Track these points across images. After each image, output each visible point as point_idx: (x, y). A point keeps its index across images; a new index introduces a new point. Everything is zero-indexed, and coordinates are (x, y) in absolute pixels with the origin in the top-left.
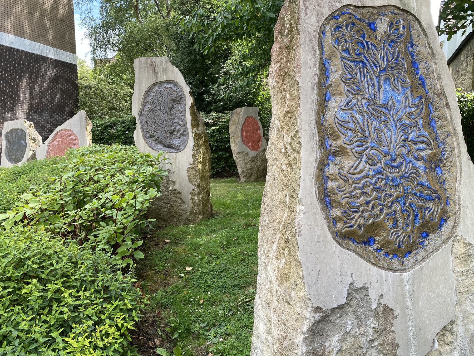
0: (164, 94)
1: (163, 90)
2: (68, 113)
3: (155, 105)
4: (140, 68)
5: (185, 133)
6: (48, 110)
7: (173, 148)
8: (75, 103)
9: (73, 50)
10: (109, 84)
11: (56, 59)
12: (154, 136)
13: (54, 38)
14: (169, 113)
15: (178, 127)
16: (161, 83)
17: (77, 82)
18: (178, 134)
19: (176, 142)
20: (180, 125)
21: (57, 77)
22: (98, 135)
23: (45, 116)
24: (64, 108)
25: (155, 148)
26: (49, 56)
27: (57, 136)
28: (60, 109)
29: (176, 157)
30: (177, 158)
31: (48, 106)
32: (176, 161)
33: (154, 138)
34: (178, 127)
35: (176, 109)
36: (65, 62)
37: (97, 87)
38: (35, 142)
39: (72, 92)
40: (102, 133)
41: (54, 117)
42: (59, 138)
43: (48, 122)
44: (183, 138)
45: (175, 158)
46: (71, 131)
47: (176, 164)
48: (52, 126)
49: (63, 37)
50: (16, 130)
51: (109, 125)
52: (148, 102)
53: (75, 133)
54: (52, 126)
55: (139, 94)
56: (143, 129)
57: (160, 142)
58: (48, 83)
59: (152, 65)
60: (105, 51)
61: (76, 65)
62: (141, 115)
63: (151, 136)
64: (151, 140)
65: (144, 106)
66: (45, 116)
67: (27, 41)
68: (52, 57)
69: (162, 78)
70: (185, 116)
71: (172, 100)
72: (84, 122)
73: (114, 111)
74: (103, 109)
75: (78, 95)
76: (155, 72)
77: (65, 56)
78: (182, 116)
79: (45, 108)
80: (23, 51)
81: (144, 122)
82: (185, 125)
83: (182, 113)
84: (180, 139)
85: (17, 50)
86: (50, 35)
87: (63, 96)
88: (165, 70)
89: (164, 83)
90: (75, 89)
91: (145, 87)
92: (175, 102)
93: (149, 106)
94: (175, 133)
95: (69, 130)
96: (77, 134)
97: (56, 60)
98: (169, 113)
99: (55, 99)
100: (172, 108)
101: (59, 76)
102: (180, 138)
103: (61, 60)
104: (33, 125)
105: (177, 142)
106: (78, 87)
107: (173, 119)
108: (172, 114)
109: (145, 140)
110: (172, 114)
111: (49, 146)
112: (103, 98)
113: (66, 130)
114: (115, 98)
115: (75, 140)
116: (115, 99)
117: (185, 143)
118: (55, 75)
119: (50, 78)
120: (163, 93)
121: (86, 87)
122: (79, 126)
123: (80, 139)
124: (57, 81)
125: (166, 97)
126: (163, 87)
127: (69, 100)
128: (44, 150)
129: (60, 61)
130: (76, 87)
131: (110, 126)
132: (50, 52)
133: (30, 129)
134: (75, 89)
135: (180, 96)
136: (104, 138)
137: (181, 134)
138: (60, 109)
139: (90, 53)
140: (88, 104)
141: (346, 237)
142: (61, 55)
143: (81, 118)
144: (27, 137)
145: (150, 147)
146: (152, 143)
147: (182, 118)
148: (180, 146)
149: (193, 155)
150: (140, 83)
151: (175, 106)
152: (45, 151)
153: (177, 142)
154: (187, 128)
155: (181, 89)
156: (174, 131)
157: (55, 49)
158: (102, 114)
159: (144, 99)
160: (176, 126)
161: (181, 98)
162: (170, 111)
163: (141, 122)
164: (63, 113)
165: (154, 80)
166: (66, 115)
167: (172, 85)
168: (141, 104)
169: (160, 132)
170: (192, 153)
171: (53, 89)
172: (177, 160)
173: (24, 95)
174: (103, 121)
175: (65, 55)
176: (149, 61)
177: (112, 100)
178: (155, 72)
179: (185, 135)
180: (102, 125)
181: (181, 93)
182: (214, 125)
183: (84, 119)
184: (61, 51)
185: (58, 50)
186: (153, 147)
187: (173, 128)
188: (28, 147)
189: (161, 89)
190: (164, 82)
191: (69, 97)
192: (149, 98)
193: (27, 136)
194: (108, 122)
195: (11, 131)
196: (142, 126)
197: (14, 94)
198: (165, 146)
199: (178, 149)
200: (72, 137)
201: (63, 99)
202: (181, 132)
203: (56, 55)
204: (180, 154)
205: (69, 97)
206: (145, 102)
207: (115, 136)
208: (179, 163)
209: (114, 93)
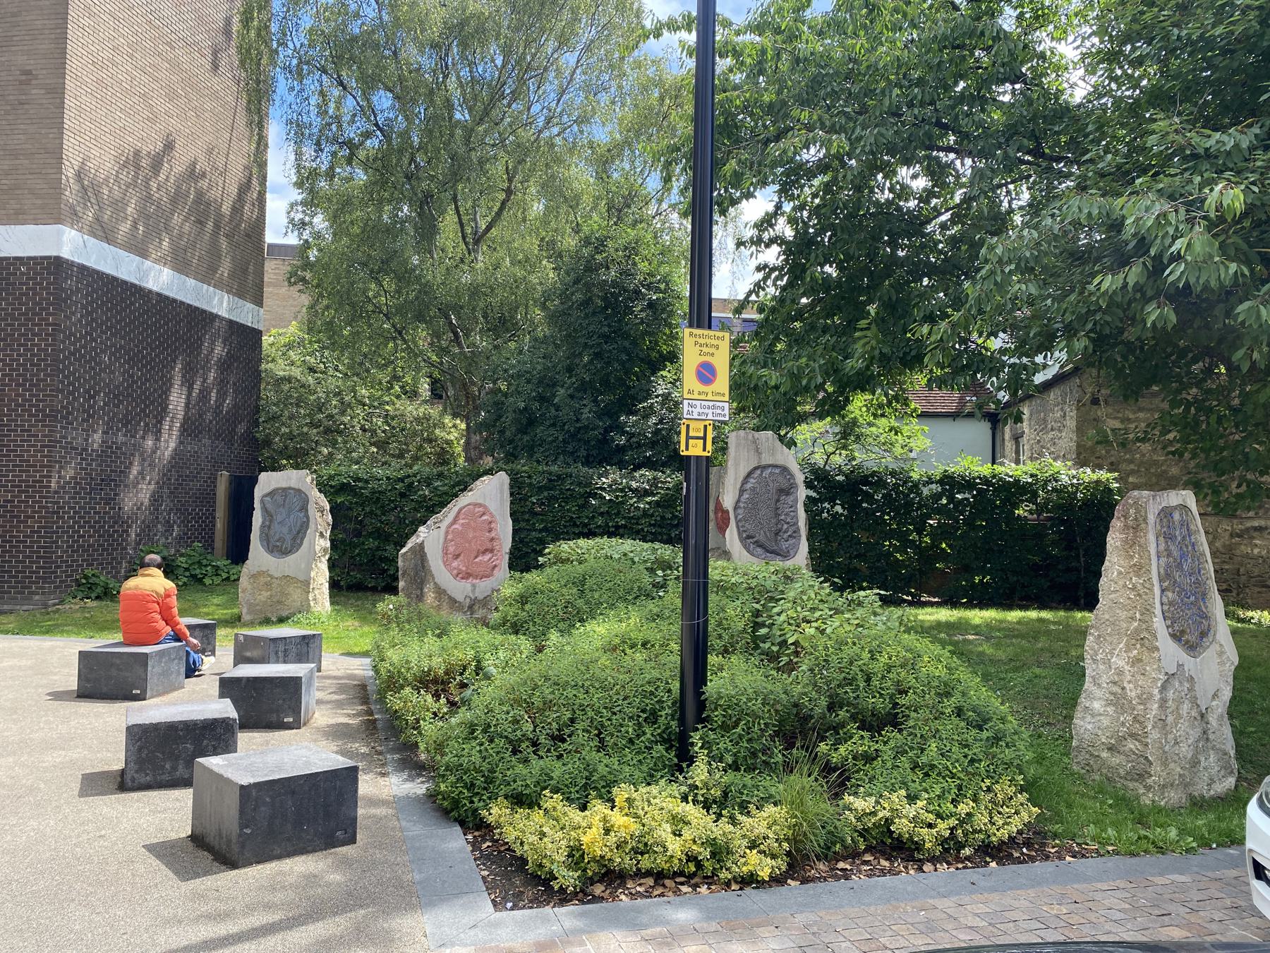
4: (738, 445)
16: (764, 467)
18: (785, 536)
19: (784, 545)
27: (462, 516)
44: (791, 541)
46: (485, 506)
49: (245, 271)
50: (285, 490)
56: (738, 527)
59: (754, 441)
67: (191, 282)
68: (223, 312)
69: (767, 459)
70: (795, 511)
76: (758, 452)
77: (246, 314)
80: (182, 303)
82: (796, 524)
85: (175, 301)
86: (225, 269)
88: (773, 451)
95: (480, 505)
100: (778, 501)
111: (447, 533)
113: (476, 505)
117: (796, 547)
132: (221, 304)
141: (1173, 636)
150: (737, 465)
152: (442, 540)
154: (798, 529)
155: (792, 476)
171: (222, 383)
173: (177, 400)
176: (750, 437)
178: (758, 452)
182: (647, 493)
188: (312, 525)
192: (748, 486)
195: (271, 494)
197: (160, 396)
200: (485, 518)
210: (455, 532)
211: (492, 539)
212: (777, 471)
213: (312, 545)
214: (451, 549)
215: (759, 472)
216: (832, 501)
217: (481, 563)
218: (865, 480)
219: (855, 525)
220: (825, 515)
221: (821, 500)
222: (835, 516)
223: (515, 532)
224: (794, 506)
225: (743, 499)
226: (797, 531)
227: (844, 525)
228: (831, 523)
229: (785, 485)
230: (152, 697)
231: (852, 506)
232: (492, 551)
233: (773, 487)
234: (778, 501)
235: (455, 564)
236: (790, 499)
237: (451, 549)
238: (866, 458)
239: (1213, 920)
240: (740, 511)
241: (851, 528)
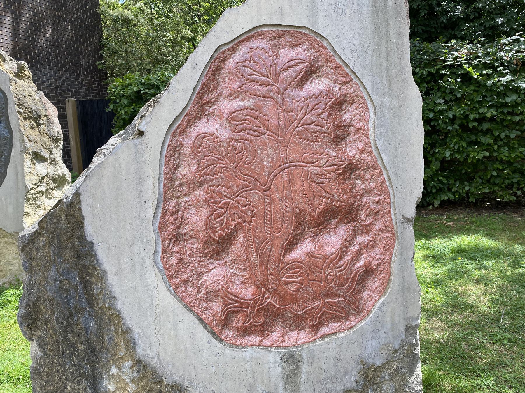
6: (49, 61)
8: (98, 51)
17: (98, 11)
23: (46, 75)
27: (227, 83)
28: (72, 62)
31: (50, 54)
38: (39, 125)
39: (92, 31)
41: (62, 77)
42: (235, 94)
43: (51, 85)
48: (60, 93)
54: (60, 93)
66: (46, 75)
75: (101, 36)
95: (295, 34)
96: (355, 65)
104: (28, 72)
111: (172, 153)
127: (87, 46)
128: (140, 180)
133: (20, 82)
138: (72, 62)
144: (13, 110)
164: (78, 69)
166: (83, 73)
188: (16, 144)
191: (87, 39)
193: (11, 105)
200: (316, 86)
210: (208, 153)
211: (349, 170)
213: (20, 174)
214: (196, 218)
217: (308, 268)
223: (434, 133)
230: (413, 46)
232: (347, 213)
235: (215, 275)
237: (196, 218)
239: (247, 157)
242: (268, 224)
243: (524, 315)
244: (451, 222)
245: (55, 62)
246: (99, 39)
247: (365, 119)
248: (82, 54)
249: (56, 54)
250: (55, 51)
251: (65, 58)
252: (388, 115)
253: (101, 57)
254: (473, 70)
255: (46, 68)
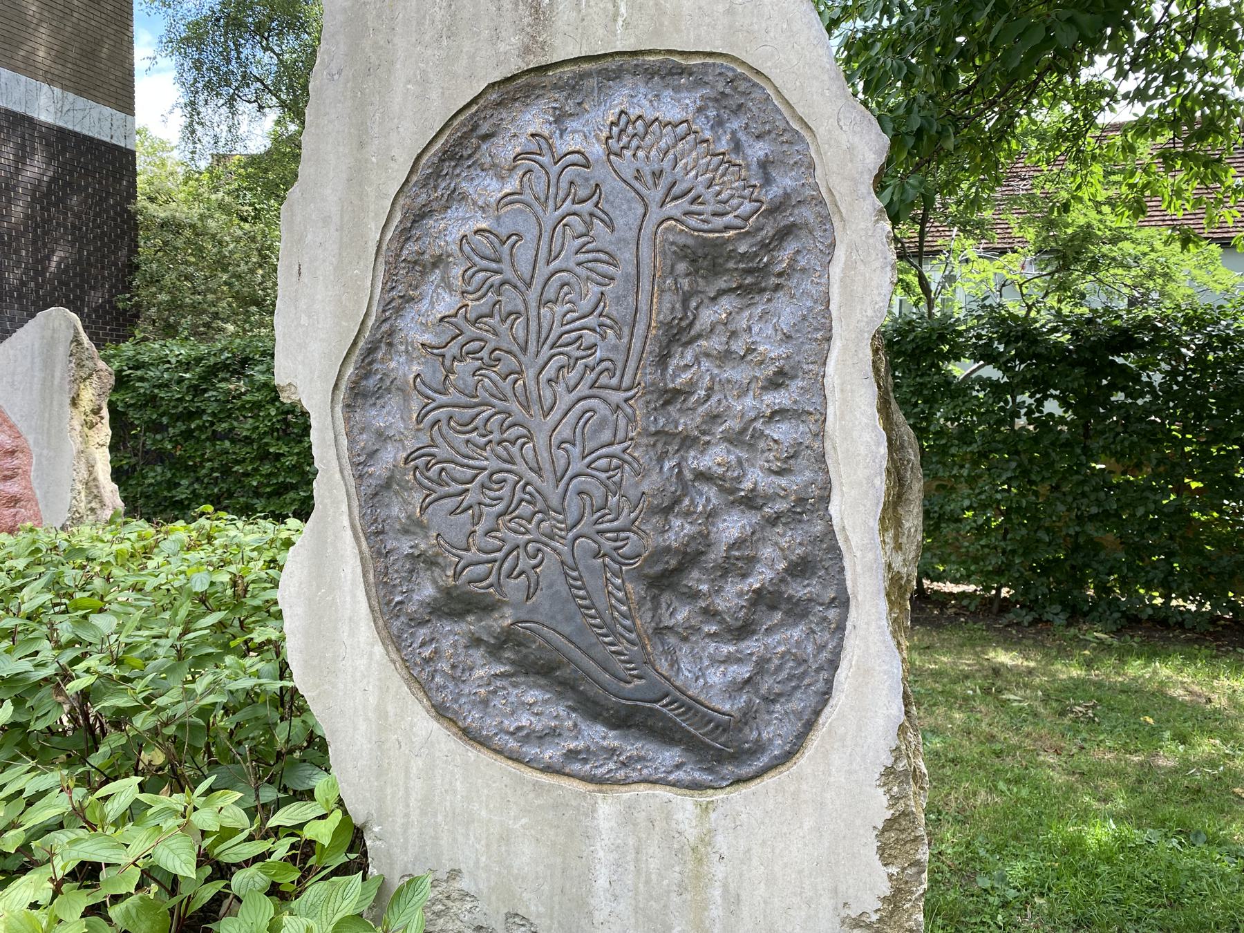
0: (611, 184)
1: (596, 150)
2: (96, 310)
3: (511, 300)
5: (799, 590)
6: (20, 297)
7: (666, 734)
9: (124, 100)
10: (245, 220)
11: (61, 124)
12: (481, 606)
13: (60, 56)
14: (649, 376)
15: (732, 526)
17: (131, 207)
18: (731, 597)
19: (709, 675)
20: (751, 502)
21: (63, 188)
22: (180, 400)
24: (83, 292)
25: (490, 725)
26: (35, 116)
29: (706, 839)
30: (722, 842)
32: (697, 880)
33: (470, 625)
34: (732, 526)
35: (715, 344)
36: (91, 139)
37: (199, 224)
40: (196, 390)
45: (700, 851)
47: (702, 906)
51: (223, 363)
52: (439, 261)
53: (14, 419)
55: (357, 177)
56: (374, 533)
57: (543, 669)
58: (31, 205)
60: (231, 106)
61: (133, 153)
62: (362, 386)
63: (456, 604)
64: (452, 634)
65: (395, 303)
70: (812, 414)
71: (684, 253)
72: (62, 367)
73: (254, 309)
74: (219, 299)
75: (134, 250)
77: (92, 119)
78: (778, 414)
79: (11, 292)
81: (391, 456)
82: (815, 502)
83: (777, 381)
84: (752, 646)
87: (80, 252)
89: (616, 75)
90: (124, 233)
91: (409, 122)
92: (715, 270)
93: (446, 303)
94: (696, 580)
96: (22, 426)
97: (61, 130)
98: (649, 376)
99: (50, 260)
100: (677, 334)
101: (70, 184)
102: (743, 631)
103: (78, 129)
105: (716, 677)
106: (136, 227)
107: (687, 442)
108: (671, 396)
109: (395, 641)
110: (671, 396)
112: (222, 263)
114: (261, 266)
115: (13, 453)
116: (260, 272)
118: (53, 180)
119: (36, 188)
120: (600, 172)
121: (164, 225)
122: (37, 386)
123: (35, 451)
124: (59, 200)
125: (627, 217)
126: (602, 114)
129: (76, 134)
130: (127, 225)
131: (225, 366)
132: (47, 105)
134: (124, 233)
135: (776, 208)
136: (200, 413)
137: (764, 599)
139: (178, 111)
140: (168, 279)
142: (79, 115)
143: (51, 344)
145: (441, 712)
146: (459, 673)
147: (782, 432)
148: (747, 717)
149: (890, 824)
151: (708, 316)
153: (716, 677)
155: (789, 137)
156: (690, 557)
157: (57, 90)
158: (216, 316)
159: (405, 235)
160: (711, 515)
161: (785, 233)
162: (663, 360)
163: (361, 462)
165: (512, 42)
167: (691, 100)
168: (364, 284)
169: (550, 563)
170: (879, 808)
172: (719, 870)
174: (203, 349)
175: (95, 113)
177: (252, 271)
179: (797, 611)
180: (198, 360)
181: (785, 181)
183: (62, 350)
184: (81, 102)
185: (71, 96)
186: (473, 718)
187: (679, 530)
189: (572, 142)
190: (609, 68)
191: (103, 256)
192: (453, 228)
194: (222, 351)
196: (373, 495)
198: (593, 709)
199: (722, 749)
201: (77, 262)
202: (760, 578)
203: (60, 111)
204: (738, 802)
205: (103, 256)
206: (407, 262)
207: (243, 406)
208: (733, 902)
209: (259, 251)
212: (673, 107)
215: (534, 118)
216: (1040, 386)
218: (1124, 339)
219: (1096, 444)
220: (1021, 422)
221: (1012, 388)
222: (1046, 424)
224: (793, 373)
225: (415, 328)
226: (820, 560)
227: (1068, 445)
228: (1035, 439)
229: (729, 208)
231: (1086, 404)
233: (636, 228)
234: (677, 334)
236: (766, 329)
238: (1104, 295)
240: (388, 416)
241: (1086, 450)
242: (579, 588)
243: (1194, 132)
244: (1190, 452)
245: (33, 297)
246: (129, 256)
247: (30, 464)
248: (89, 283)
249: (37, 284)
250: (35, 279)
251: (55, 289)
252: (45, 463)
253: (127, 288)
254: (1157, 833)
255: (13, 308)
